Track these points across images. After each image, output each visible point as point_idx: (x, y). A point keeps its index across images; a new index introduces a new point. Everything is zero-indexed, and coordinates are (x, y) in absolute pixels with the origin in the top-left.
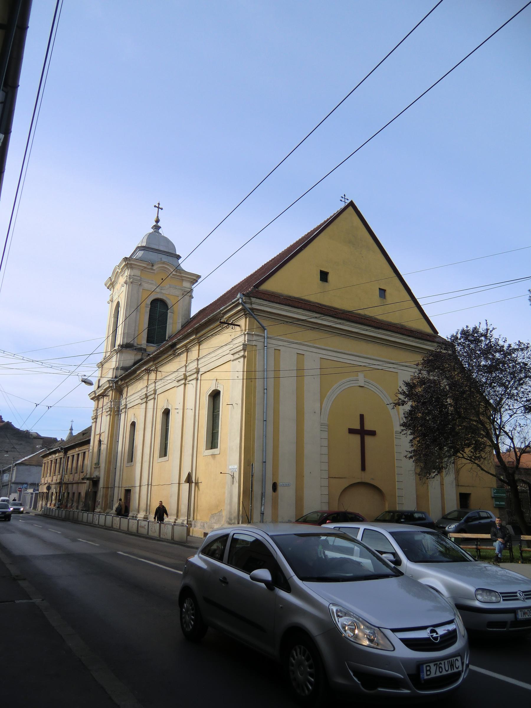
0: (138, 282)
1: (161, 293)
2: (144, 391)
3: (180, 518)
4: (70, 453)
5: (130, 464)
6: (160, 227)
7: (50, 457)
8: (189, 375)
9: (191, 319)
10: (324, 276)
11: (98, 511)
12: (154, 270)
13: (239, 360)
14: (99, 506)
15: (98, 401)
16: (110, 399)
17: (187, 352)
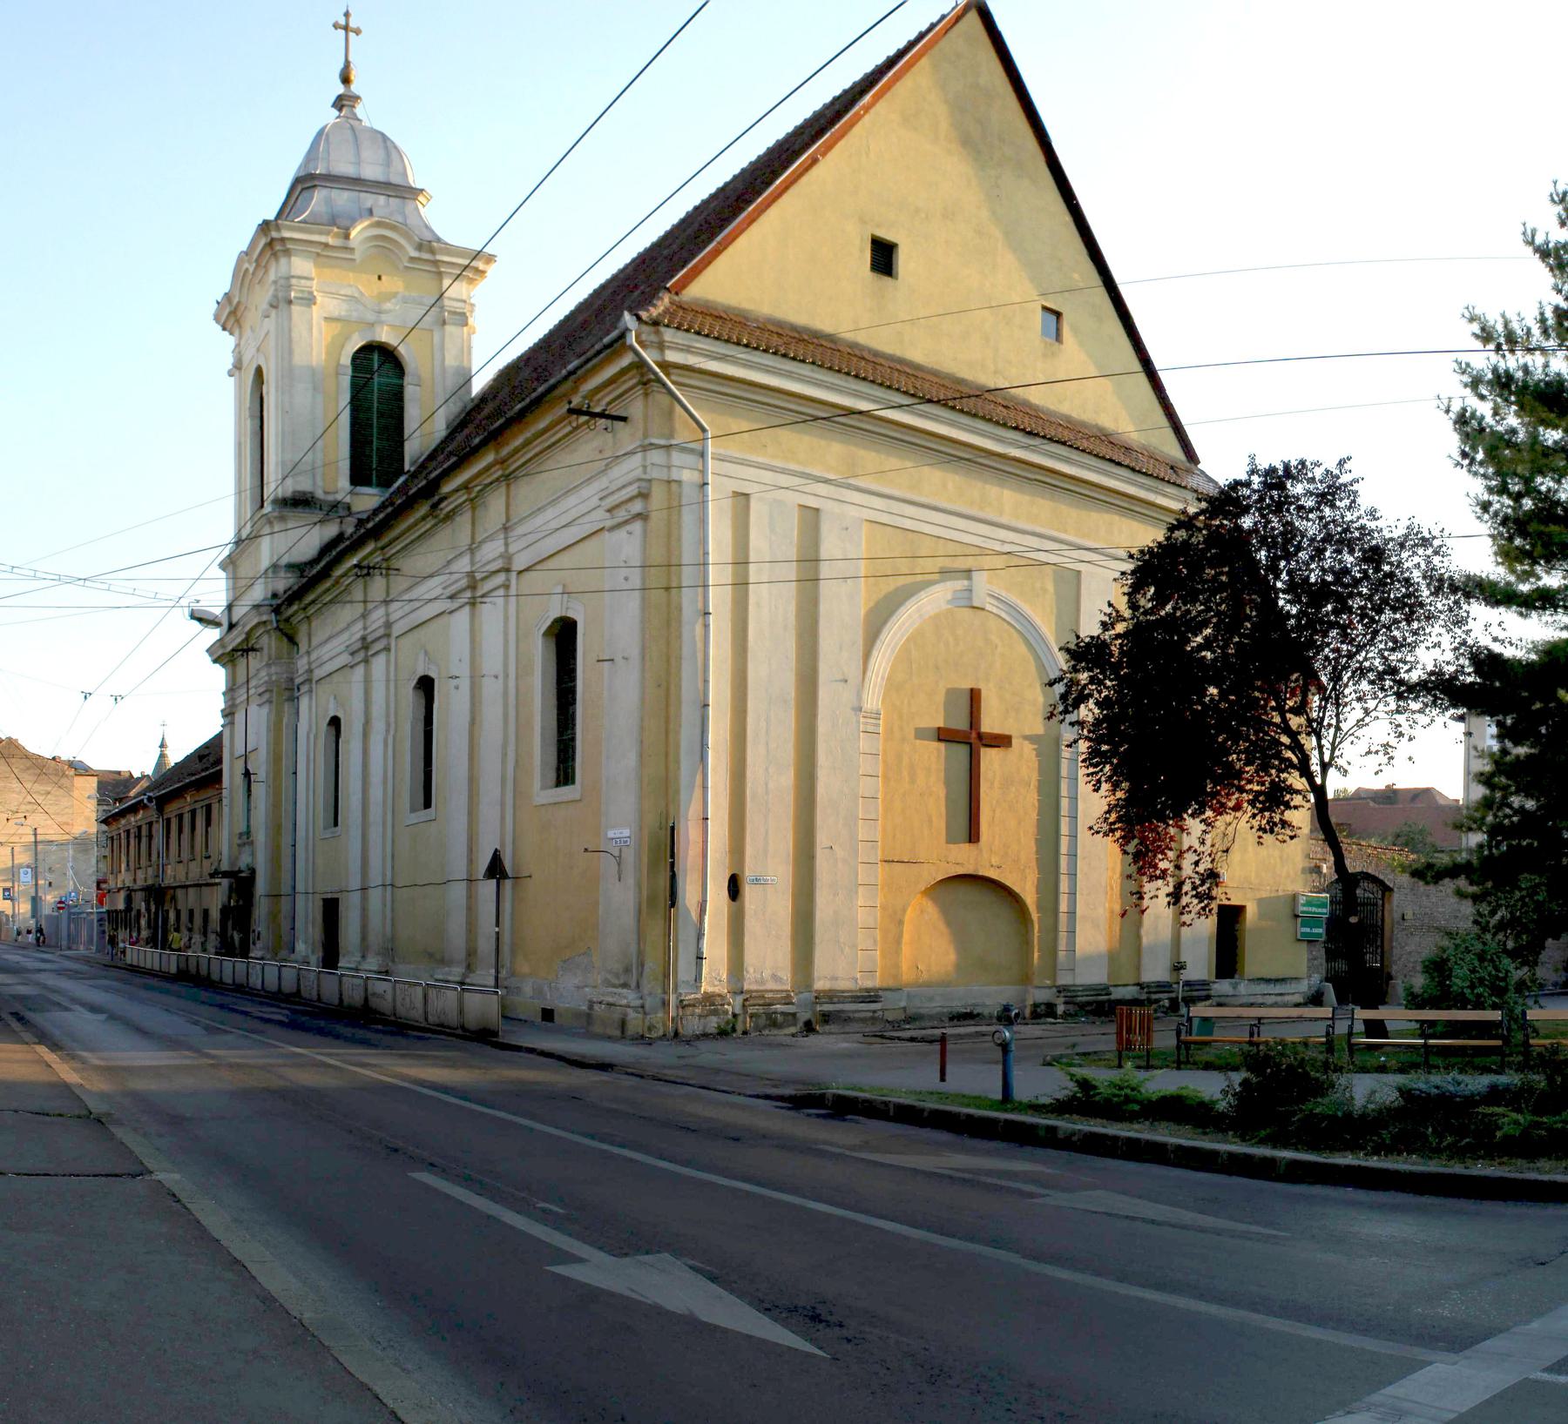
2: (357, 631)
3: (478, 972)
4: (172, 809)
5: (332, 833)
7: (123, 822)
9: (472, 400)
10: (883, 256)
11: (258, 956)
12: (353, 249)
13: (628, 527)
14: (259, 944)
15: (234, 666)
16: (266, 659)
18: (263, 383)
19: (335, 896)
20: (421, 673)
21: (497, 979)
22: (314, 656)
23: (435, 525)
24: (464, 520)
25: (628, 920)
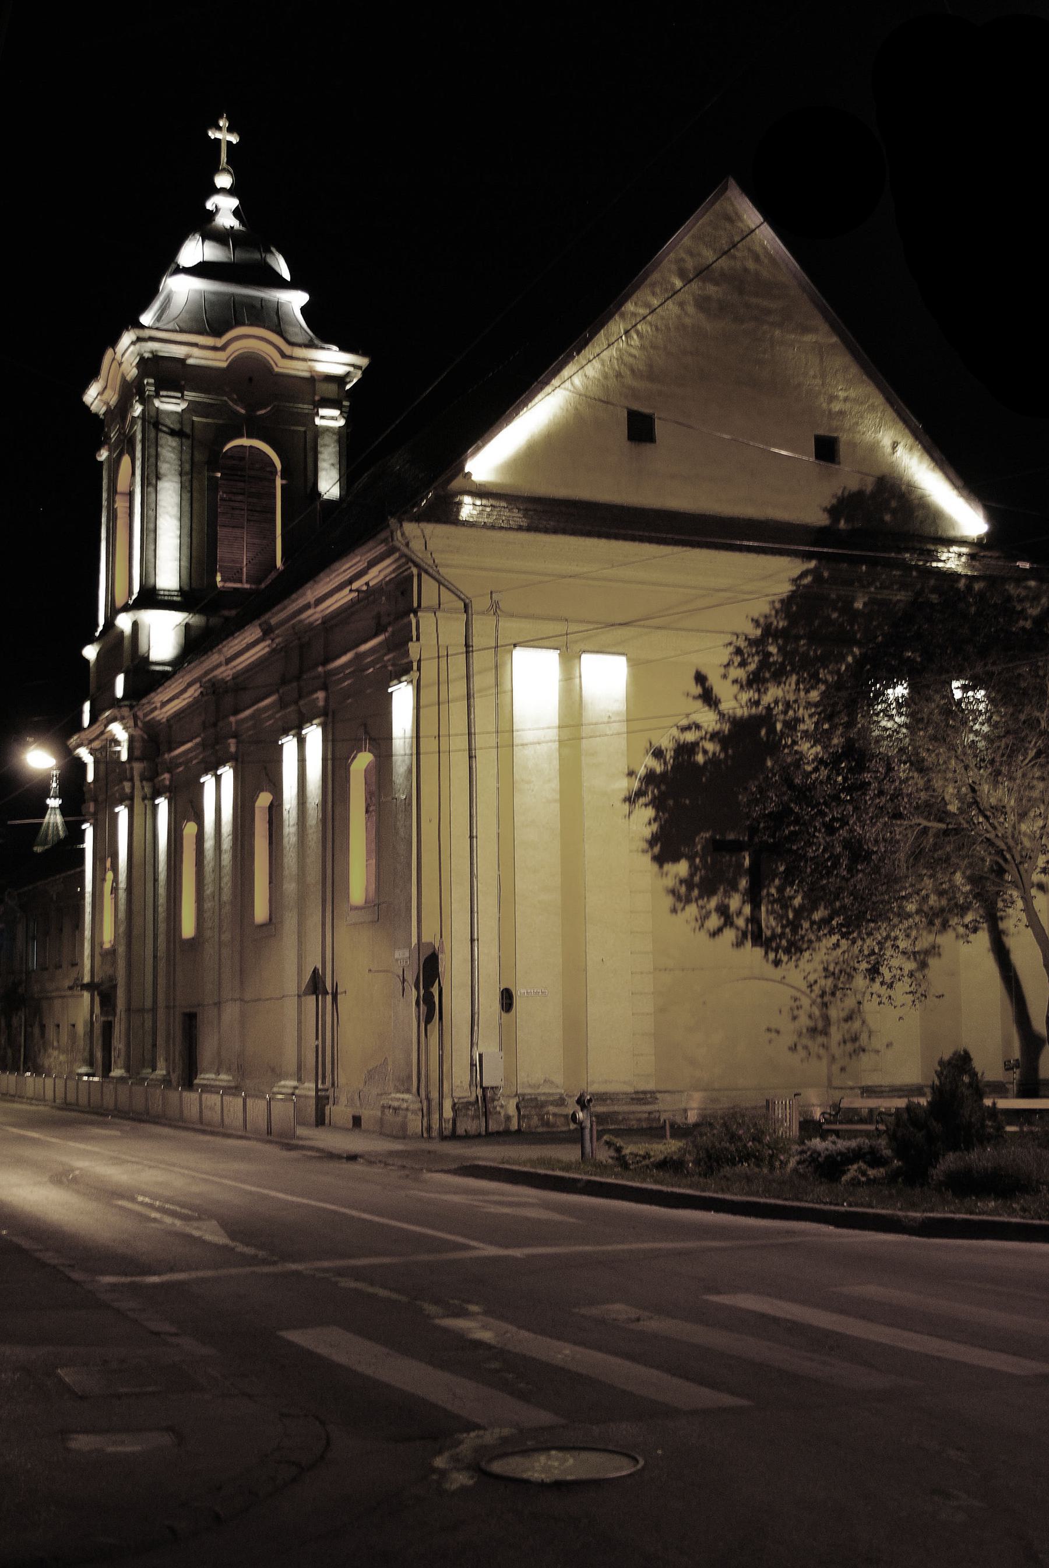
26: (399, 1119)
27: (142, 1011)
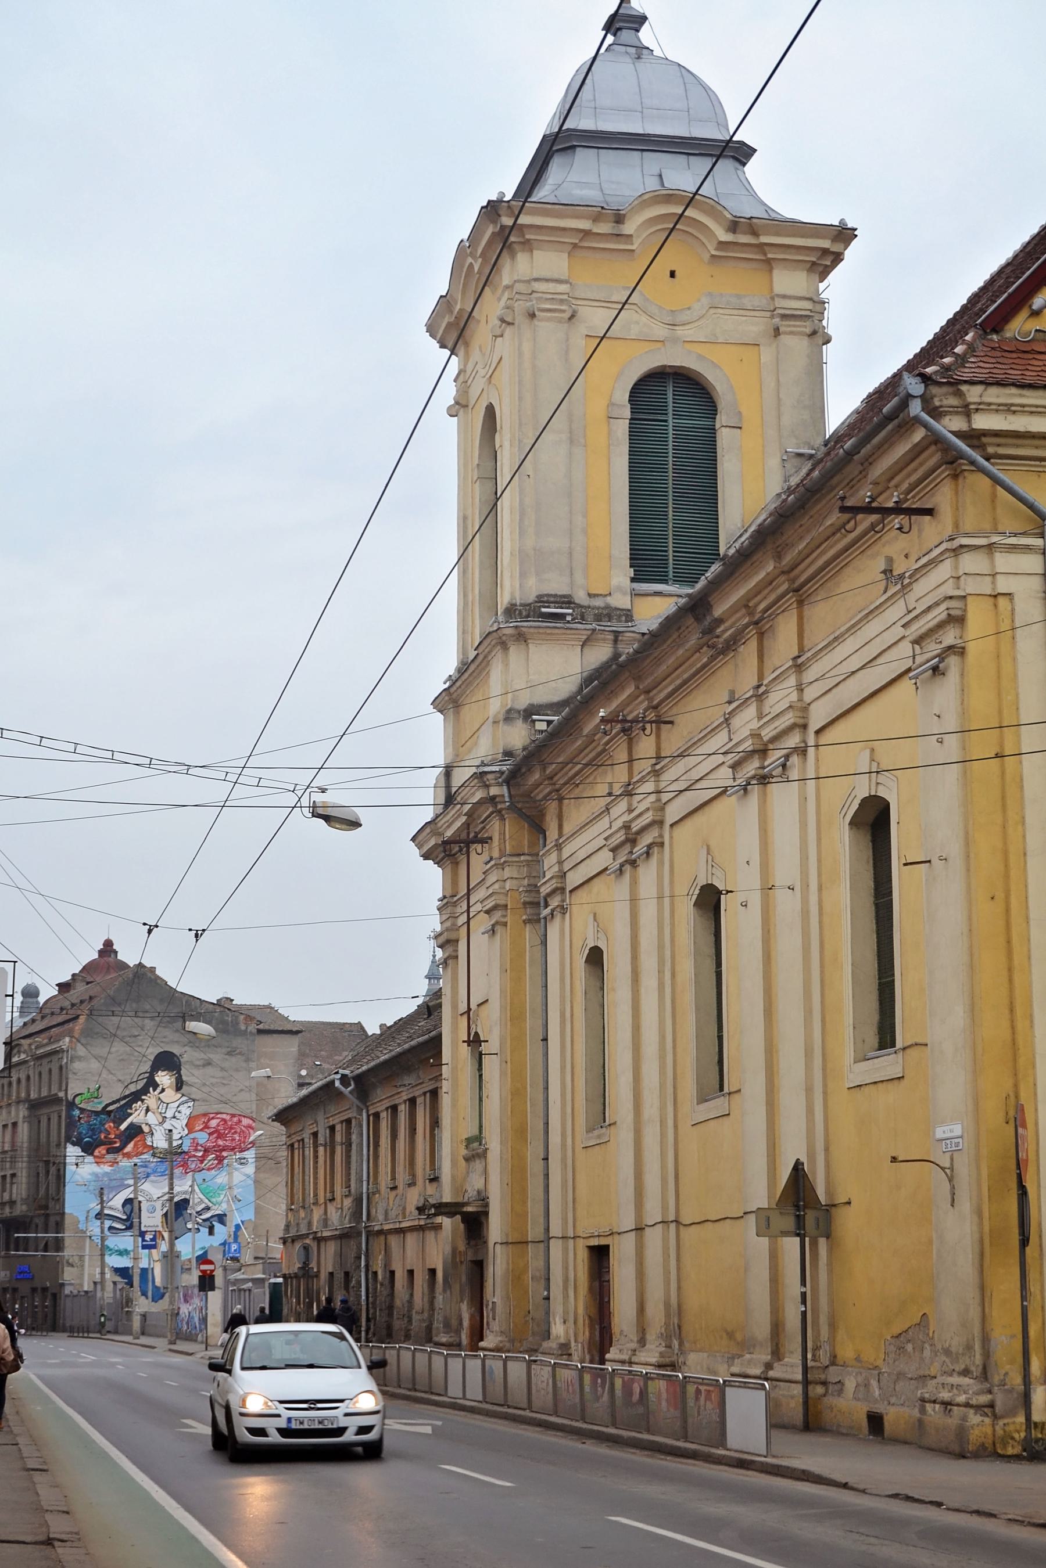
0: (563, 307)
1: (675, 340)
3: (786, 1360)
6: (642, 19)
8: (771, 735)
12: (631, 236)
17: (761, 635)
18: (495, 430)
19: (603, 1242)
20: (702, 881)
21: (805, 1369)
22: (566, 851)
23: (713, 658)
24: (749, 650)
25: (965, 1265)
26: (953, 1422)
27: (188, 769)
